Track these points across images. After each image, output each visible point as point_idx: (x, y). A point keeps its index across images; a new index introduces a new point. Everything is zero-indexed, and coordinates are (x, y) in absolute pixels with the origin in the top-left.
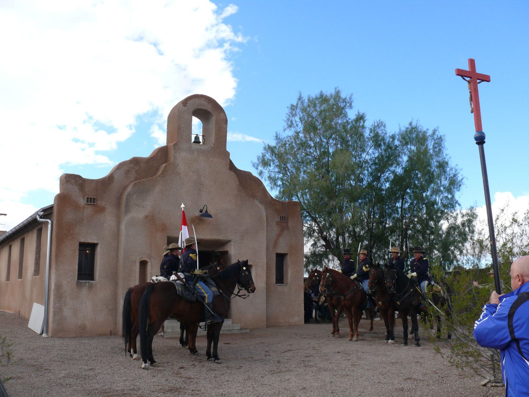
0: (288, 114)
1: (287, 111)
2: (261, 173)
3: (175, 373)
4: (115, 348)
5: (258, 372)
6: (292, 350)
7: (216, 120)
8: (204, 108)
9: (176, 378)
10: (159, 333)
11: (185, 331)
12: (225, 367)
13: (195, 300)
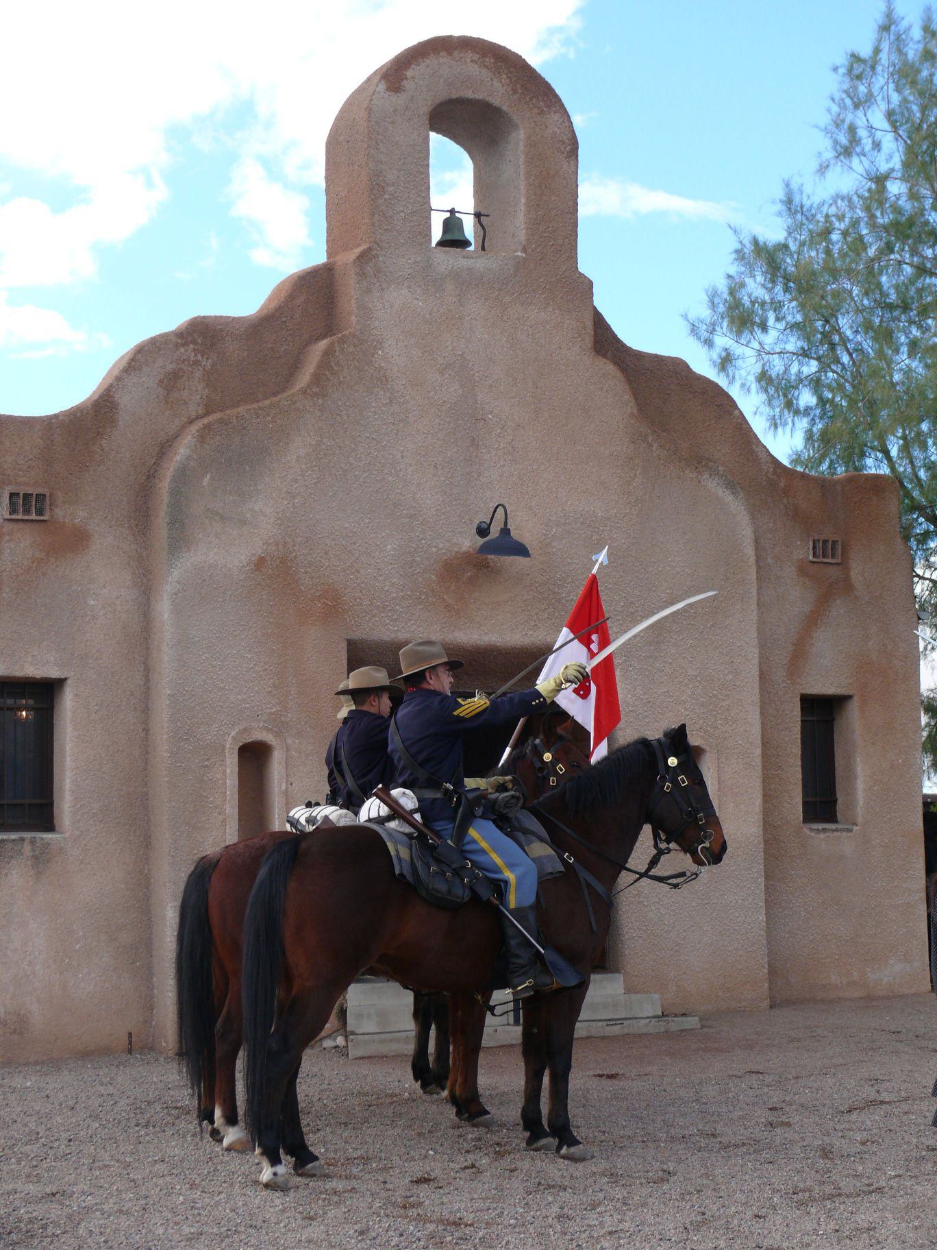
0: (837, 98)
1: (834, 84)
2: (726, 362)
3: (394, 1204)
4: (149, 1103)
5: (742, 1198)
6: (882, 1102)
9: (402, 1224)
10: (329, 1036)
11: (433, 1027)
12: (603, 1175)
13: (466, 899)
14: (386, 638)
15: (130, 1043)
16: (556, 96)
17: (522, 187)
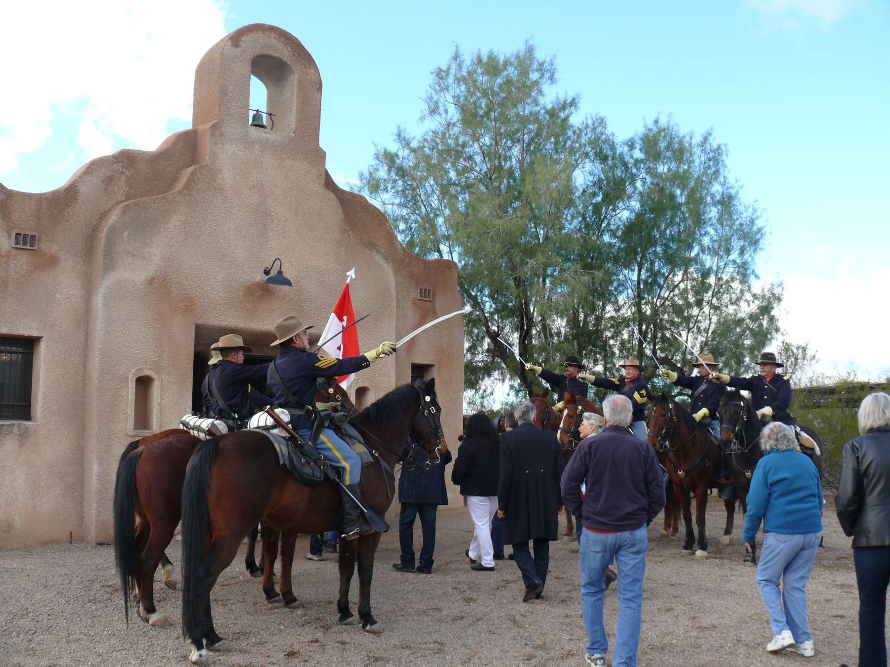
0: (432, 86)
1: (431, 79)
7: (300, 82)
8: (277, 55)
14: (216, 324)
15: (71, 538)
16: (313, 60)
17: (295, 102)
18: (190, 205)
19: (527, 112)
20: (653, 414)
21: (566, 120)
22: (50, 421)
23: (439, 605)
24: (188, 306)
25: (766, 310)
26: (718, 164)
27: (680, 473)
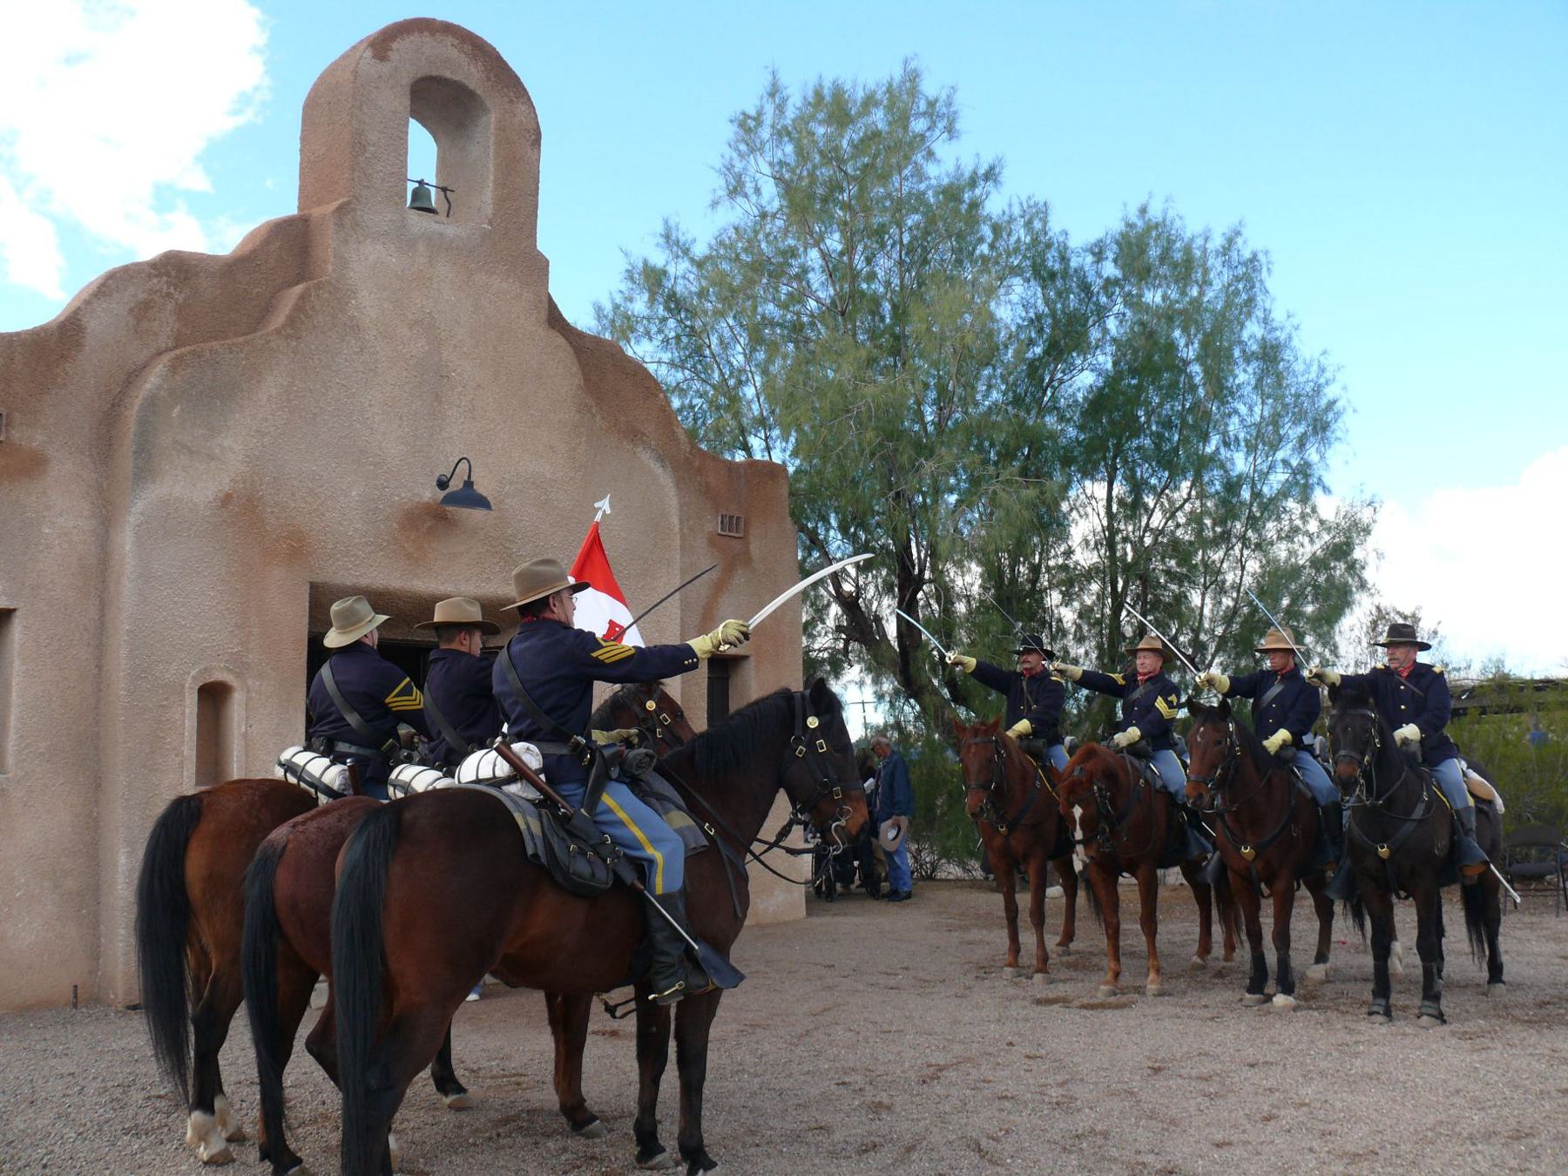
1: (730, 131)
14: (348, 583)
15: (76, 996)
16: (525, 90)
18: (298, 356)
19: (905, 190)
20: (1199, 739)
21: (975, 205)
22: (33, 771)
23: (826, 1119)
24: (297, 548)
25: (1341, 550)
26: (1253, 287)
27: (1247, 851)
